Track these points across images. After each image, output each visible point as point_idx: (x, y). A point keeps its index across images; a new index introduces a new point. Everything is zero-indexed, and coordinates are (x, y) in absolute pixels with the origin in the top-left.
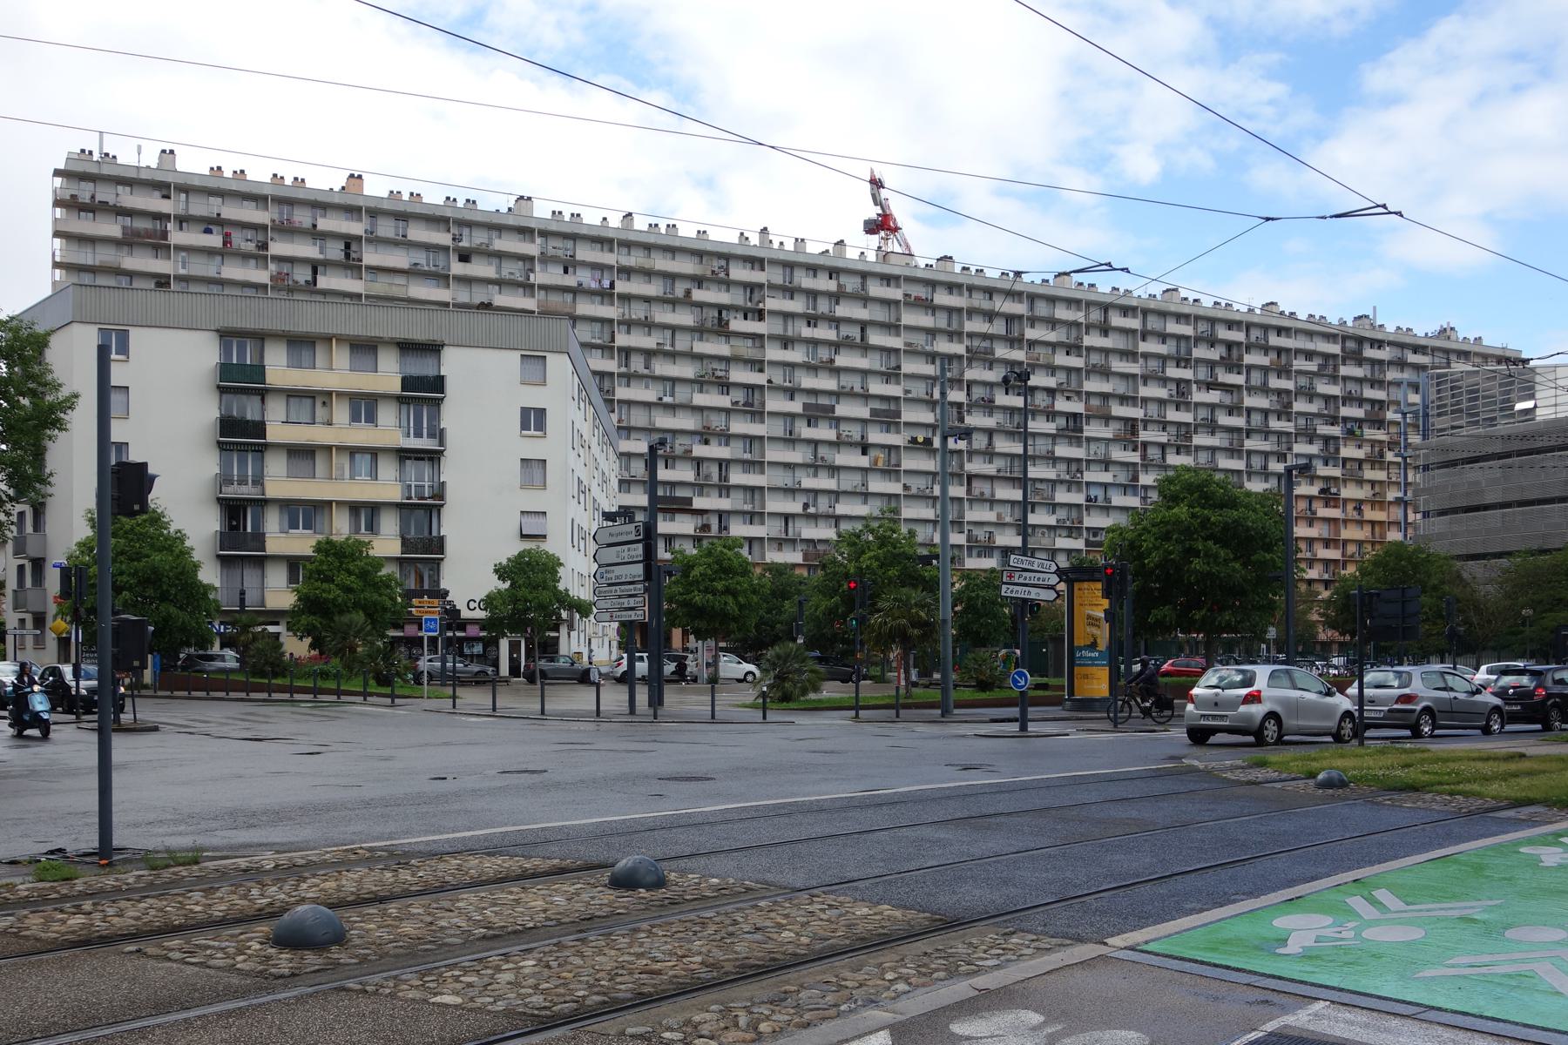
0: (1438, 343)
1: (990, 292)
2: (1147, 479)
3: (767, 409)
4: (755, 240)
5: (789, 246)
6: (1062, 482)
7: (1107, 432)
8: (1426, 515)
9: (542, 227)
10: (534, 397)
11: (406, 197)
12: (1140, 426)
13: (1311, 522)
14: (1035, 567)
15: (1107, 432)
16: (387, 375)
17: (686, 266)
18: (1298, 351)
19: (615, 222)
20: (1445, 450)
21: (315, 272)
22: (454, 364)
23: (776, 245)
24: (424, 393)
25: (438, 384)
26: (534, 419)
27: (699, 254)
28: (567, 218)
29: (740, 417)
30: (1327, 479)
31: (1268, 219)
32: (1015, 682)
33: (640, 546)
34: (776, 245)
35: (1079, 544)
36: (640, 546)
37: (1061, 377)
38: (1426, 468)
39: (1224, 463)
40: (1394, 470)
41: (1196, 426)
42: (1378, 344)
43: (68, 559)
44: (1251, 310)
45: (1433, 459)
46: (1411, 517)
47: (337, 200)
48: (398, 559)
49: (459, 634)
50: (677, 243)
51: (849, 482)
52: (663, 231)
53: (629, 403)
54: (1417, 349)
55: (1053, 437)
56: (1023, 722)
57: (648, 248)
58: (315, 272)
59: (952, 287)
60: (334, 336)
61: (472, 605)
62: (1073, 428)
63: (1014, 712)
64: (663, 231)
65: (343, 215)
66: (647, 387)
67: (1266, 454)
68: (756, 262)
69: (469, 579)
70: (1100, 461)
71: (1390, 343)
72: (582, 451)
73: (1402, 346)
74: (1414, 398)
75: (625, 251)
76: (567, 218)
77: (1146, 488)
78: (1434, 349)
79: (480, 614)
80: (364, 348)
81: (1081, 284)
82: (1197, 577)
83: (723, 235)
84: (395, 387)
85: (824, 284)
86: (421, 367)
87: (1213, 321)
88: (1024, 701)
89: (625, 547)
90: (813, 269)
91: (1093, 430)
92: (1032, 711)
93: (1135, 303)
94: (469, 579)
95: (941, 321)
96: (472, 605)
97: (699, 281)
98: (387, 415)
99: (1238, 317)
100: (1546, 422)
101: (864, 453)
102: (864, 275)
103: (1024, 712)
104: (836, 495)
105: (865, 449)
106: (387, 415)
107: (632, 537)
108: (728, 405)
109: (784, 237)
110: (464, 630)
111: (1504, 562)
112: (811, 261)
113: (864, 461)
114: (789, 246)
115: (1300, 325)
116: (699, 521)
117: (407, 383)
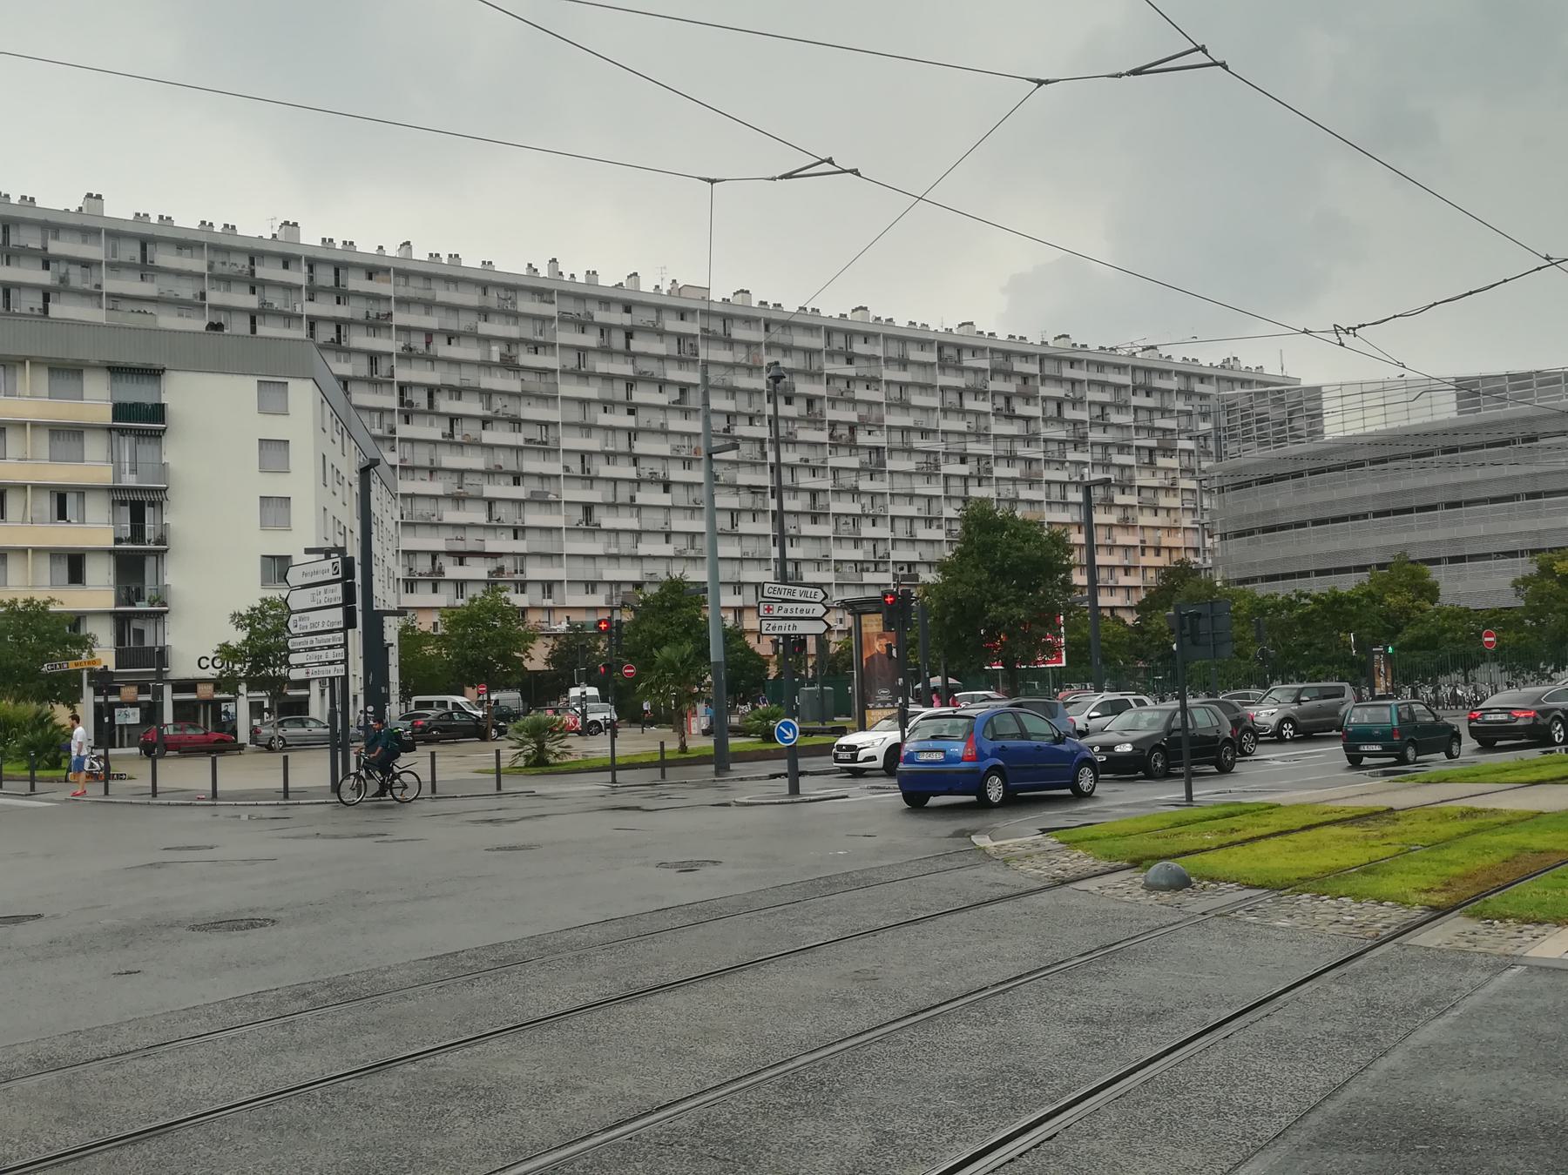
0: (1223, 373)
1: (787, 325)
2: (949, 512)
3: (563, 446)
4: (544, 272)
5: (581, 278)
6: (867, 516)
7: (909, 465)
8: (1224, 537)
9: (310, 254)
10: (275, 428)
11: (154, 220)
12: (941, 458)
13: (1111, 548)
14: (797, 597)
15: (909, 465)
16: (95, 401)
17: (471, 298)
18: (1091, 383)
19: (392, 251)
20: (1237, 472)
21: (46, 299)
22: (183, 393)
23: (567, 278)
24: (142, 422)
25: (157, 412)
26: (274, 451)
27: (484, 286)
28: (339, 246)
29: (534, 455)
30: (1125, 507)
31: (1040, 83)
32: (781, 735)
33: (339, 586)
34: (567, 278)
35: (886, 578)
36: (339, 586)
37: (863, 410)
38: (1221, 490)
39: (1025, 493)
40: (1188, 496)
41: (996, 458)
42: (1164, 373)
43: (88, 636)
44: (1044, 343)
45: (1228, 481)
46: (1208, 542)
47: (71, 221)
48: (111, 613)
49: (112, 699)
50: (460, 274)
51: (654, 520)
52: (445, 261)
53: (412, 441)
54: (1203, 378)
55: (857, 470)
56: (794, 776)
57: (428, 277)
58: (46, 299)
59: (749, 320)
60: (28, 358)
61: (204, 663)
62: (875, 464)
63: (781, 766)
64: (445, 261)
65: (78, 238)
66: (431, 424)
67: (1063, 484)
68: (542, 293)
69: (196, 638)
70: (905, 495)
71: (1178, 373)
72: (338, 489)
73: (1188, 376)
74: (1205, 426)
75: (402, 281)
76: (339, 246)
77: (949, 520)
78: (1219, 379)
79: (211, 673)
80: (66, 371)
81: (878, 319)
82: (991, 603)
83: (510, 264)
84: (106, 417)
85: (617, 317)
86: (136, 393)
87: (1008, 354)
88: (793, 753)
89: (322, 588)
90: (606, 302)
91: (894, 463)
92: (804, 764)
93: (931, 337)
94: (196, 638)
95: (740, 356)
96: (204, 663)
97: (484, 313)
98: (95, 447)
99: (1031, 350)
100: (1335, 441)
101: (666, 490)
102: (659, 309)
103: (793, 765)
104: (638, 534)
105: (667, 486)
106: (95, 447)
107: (329, 576)
108: (521, 443)
109: (575, 269)
110: (194, 690)
111: (744, 800)
112: (604, 294)
113: (666, 499)
114: (581, 278)
115: (1091, 357)
116: (491, 565)
117: (120, 411)
